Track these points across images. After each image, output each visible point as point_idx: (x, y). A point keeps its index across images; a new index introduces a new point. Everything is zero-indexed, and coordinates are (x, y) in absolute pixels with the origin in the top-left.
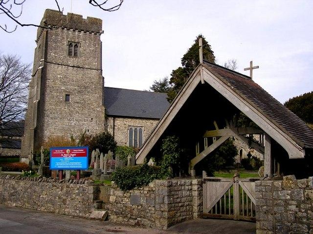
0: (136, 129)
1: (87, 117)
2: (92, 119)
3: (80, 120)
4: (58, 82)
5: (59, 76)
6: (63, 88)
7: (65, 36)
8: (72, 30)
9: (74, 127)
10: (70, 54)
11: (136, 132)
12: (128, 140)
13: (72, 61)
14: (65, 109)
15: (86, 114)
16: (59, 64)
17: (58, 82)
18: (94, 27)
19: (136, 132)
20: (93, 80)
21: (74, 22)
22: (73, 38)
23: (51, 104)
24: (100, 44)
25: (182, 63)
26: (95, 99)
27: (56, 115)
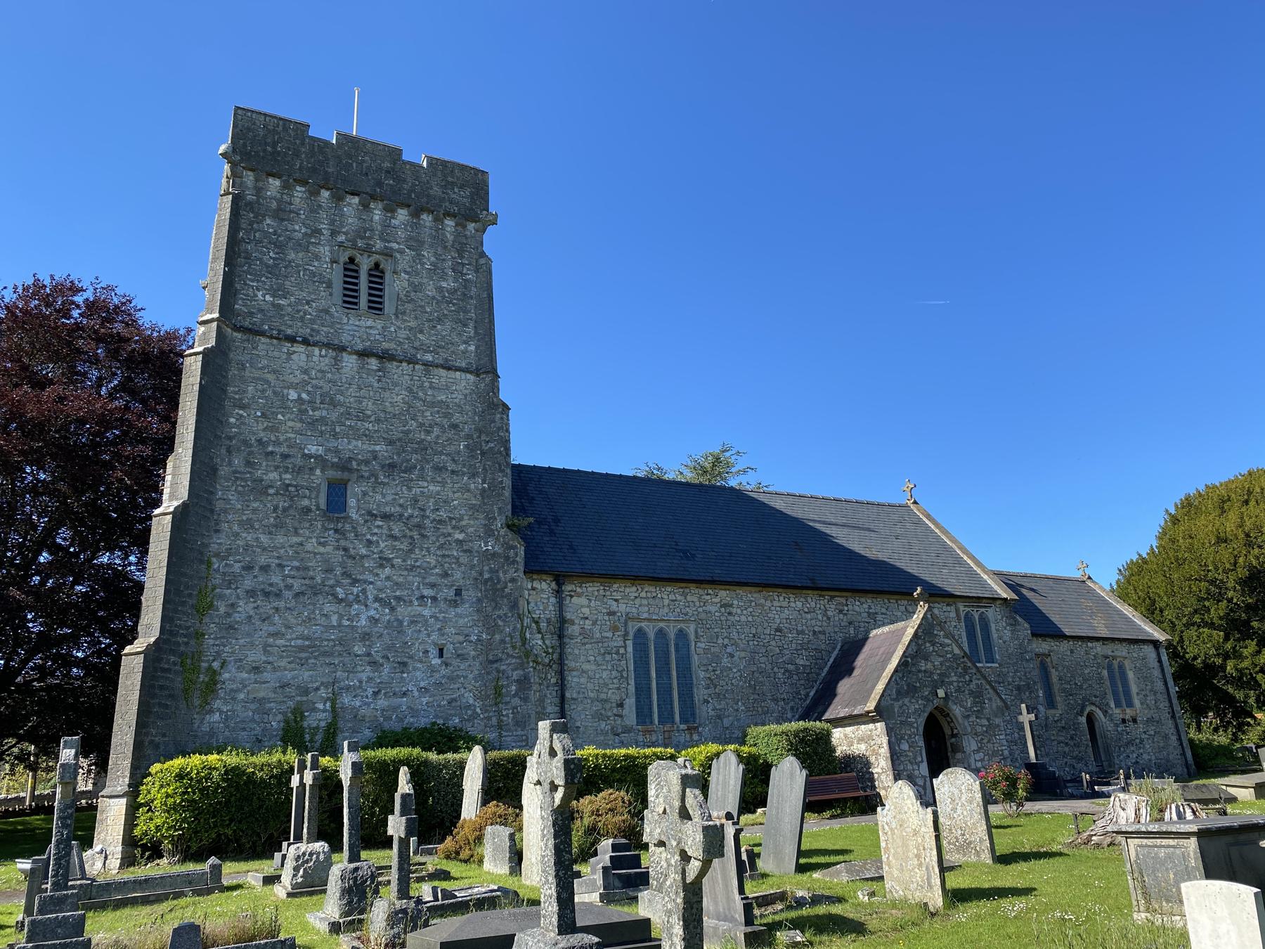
0: (661, 633)
1: (433, 586)
2: (458, 592)
3: (398, 599)
4: (289, 424)
5: (293, 395)
6: (313, 449)
7: (328, 227)
8: (356, 200)
9: (366, 637)
10: (350, 300)
11: (666, 717)
12: (632, 688)
13: (360, 327)
14: (317, 544)
15: (427, 569)
16: (292, 339)
17: (289, 424)
18: (458, 197)
19: (666, 717)
20: (457, 418)
21: (361, 171)
22: (361, 233)
23: (248, 525)
24: (484, 268)
25: (1188, 498)
26: (462, 507)
27: (276, 579)
